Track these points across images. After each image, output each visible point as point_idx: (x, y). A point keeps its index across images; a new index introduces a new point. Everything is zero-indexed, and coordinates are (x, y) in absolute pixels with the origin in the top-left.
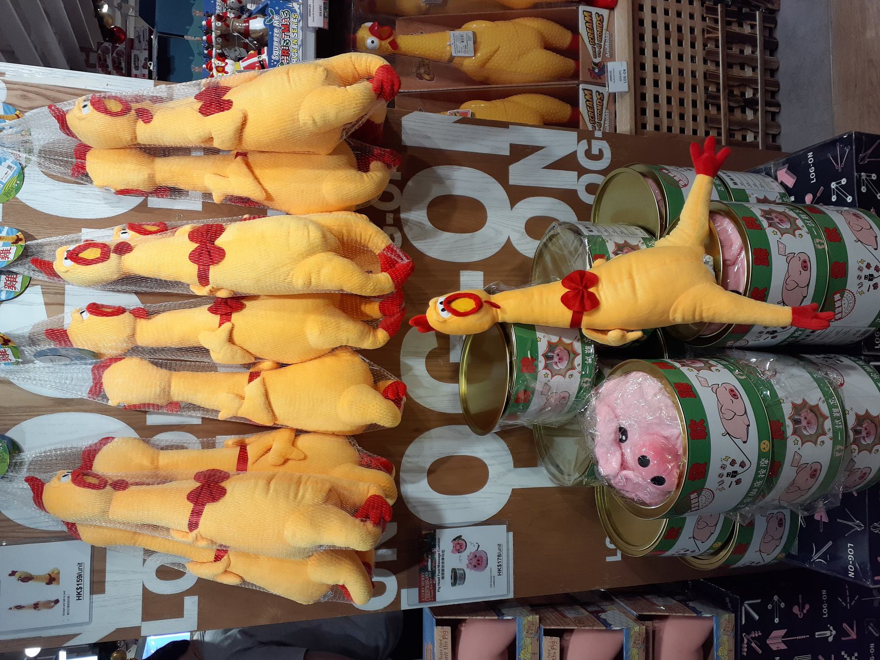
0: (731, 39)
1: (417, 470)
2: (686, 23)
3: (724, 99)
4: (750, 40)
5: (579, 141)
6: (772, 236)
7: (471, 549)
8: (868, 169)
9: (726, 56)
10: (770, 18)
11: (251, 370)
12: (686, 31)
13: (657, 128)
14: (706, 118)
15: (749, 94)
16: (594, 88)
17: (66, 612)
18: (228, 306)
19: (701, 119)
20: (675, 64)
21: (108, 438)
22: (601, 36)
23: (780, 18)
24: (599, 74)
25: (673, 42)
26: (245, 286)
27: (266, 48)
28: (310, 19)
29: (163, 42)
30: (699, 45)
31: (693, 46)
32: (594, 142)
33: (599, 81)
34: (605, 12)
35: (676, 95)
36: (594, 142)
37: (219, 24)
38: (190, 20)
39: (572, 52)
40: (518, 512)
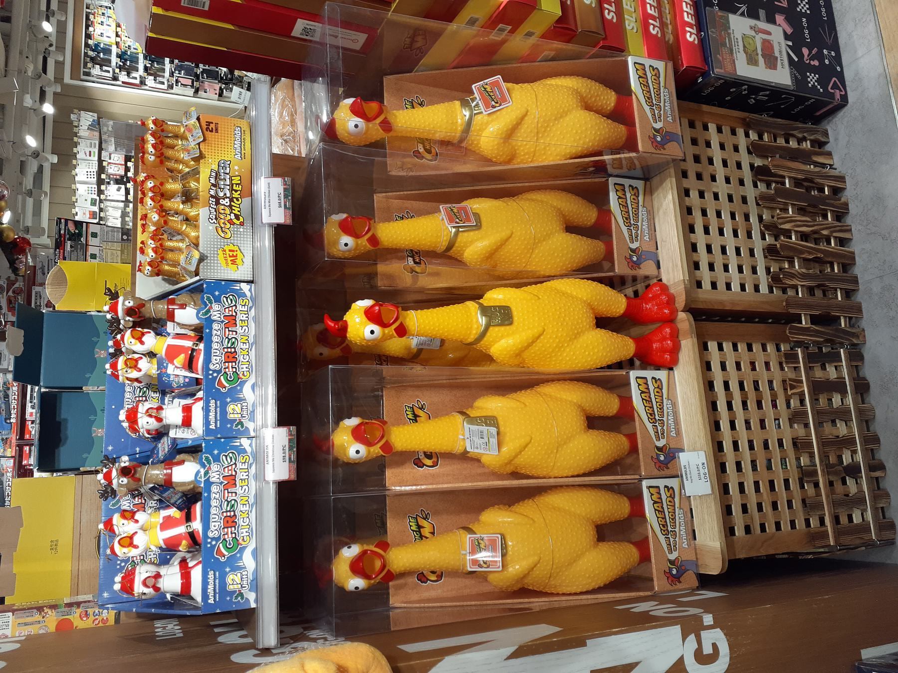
0: (819, 388)
3: (823, 475)
4: (838, 386)
5: (684, 640)
9: (818, 413)
10: (856, 357)
11: (197, 278)
12: (764, 387)
13: (748, 529)
14: (804, 501)
15: (847, 459)
16: (661, 483)
19: (797, 504)
22: (662, 409)
23: (868, 353)
24: (666, 461)
27: (198, 506)
28: (269, 468)
29: (48, 405)
30: (781, 402)
32: (704, 634)
33: (666, 472)
34: (662, 374)
35: (764, 478)
36: (704, 634)
37: (125, 480)
38: (92, 364)
39: (618, 421)
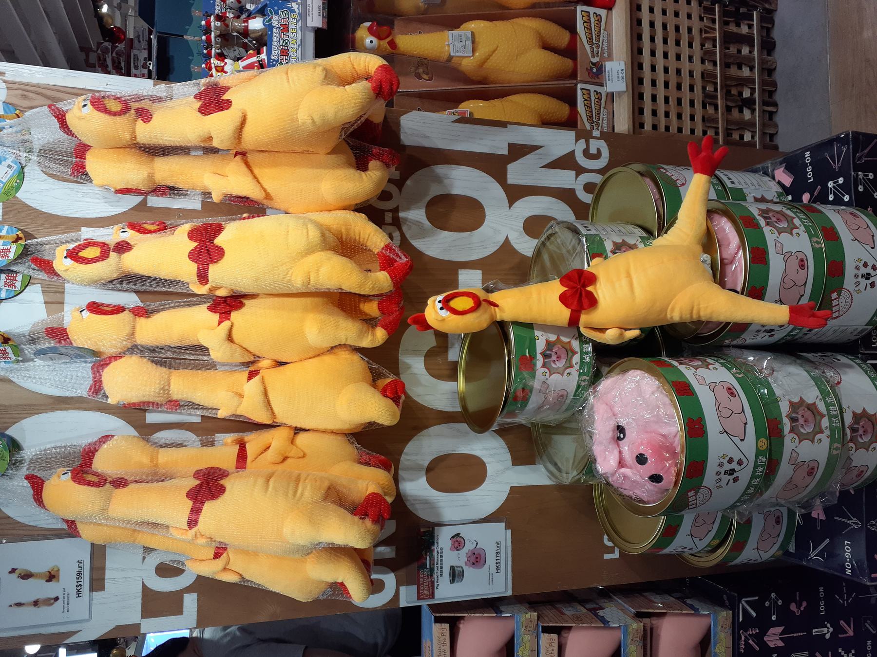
0: (729, 39)
1: (416, 468)
2: (684, 23)
3: (722, 99)
4: (748, 40)
5: (577, 141)
6: (770, 235)
7: (469, 547)
8: (865, 168)
9: (724, 56)
10: (768, 18)
12: (684, 31)
13: (655, 127)
14: (703, 117)
15: (746, 94)
16: (592, 88)
17: (66, 609)
18: (228, 304)
19: (698, 118)
20: (672, 64)
21: (107, 436)
22: (599, 36)
23: (778, 18)
24: (597, 74)
25: (671, 41)
26: (244, 285)
27: (265, 48)
28: (309, 19)
29: (163, 42)
30: (696, 44)
31: (690, 45)
32: (591, 141)
33: (597, 80)
34: (603, 12)
35: (673, 95)
36: (591, 141)
37: (219, 24)
38: (189, 20)
40: (516, 510)
